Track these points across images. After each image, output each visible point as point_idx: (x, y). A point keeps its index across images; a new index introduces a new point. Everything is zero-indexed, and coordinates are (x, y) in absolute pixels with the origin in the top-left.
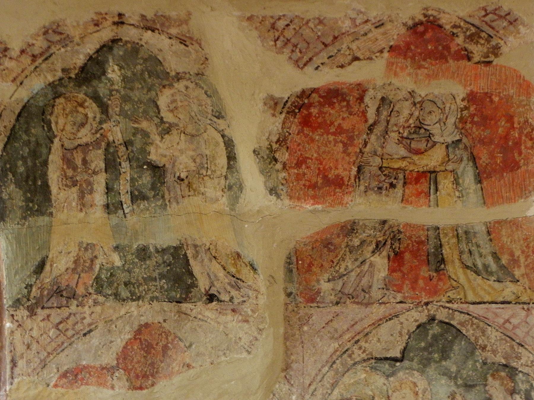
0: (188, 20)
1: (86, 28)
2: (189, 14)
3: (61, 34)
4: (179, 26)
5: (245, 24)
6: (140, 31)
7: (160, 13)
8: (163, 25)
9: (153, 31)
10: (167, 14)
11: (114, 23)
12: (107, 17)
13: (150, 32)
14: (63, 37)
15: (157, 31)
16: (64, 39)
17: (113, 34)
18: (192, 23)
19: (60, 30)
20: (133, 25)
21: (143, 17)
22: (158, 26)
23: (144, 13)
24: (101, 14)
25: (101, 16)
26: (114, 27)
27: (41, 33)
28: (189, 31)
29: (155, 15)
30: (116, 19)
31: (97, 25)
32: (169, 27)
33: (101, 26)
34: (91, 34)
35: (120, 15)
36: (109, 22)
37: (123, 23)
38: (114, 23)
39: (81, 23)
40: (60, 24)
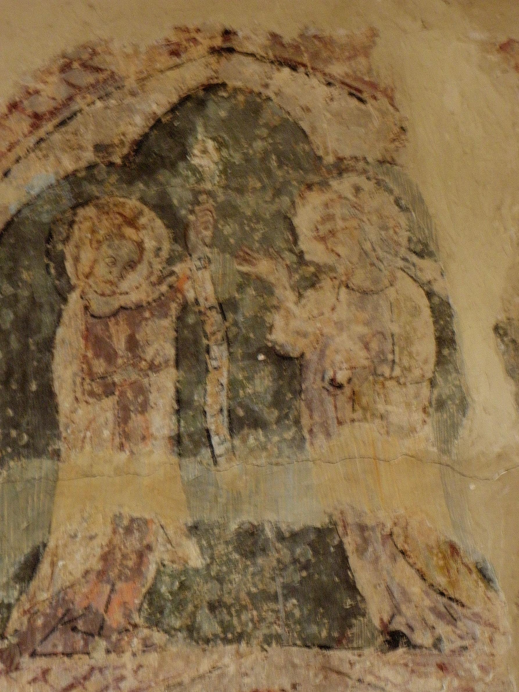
0: (370, 47)
1: (151, 60)
2: (373, 34)
3: (98, 70)
4: (349, 58)
5: (494, 58)
6: (267, 67)
7: (312, 31)
8: (315, 56)
9: (294, 68)
10: (326, 34)
11: (214, 51)
12: (199, 37)
13: (286, 71)
14: (101, 76)
15: (302, 69)
16: (105, 81)
17: (210, 73)
18: (376, 53)
19: (96, 62)
20: (253, 55)
21: (275, 37)
22: (305, 59)
23: (278, 31)
24: (187, 30)
25: (187, 35)
26: (212, 59)
27: (55, 68)
28: (370, 71)
29: (302, 36)
30: (218, 42)
31: (175, 53)
32: (328, 61)
33: (184, 57)
34: (162, 71)
35: (227, 34)
36: (202, 49)
37: (231, 50)
38: (214, 51)
39: (143, 49)
40: (99, 49)
